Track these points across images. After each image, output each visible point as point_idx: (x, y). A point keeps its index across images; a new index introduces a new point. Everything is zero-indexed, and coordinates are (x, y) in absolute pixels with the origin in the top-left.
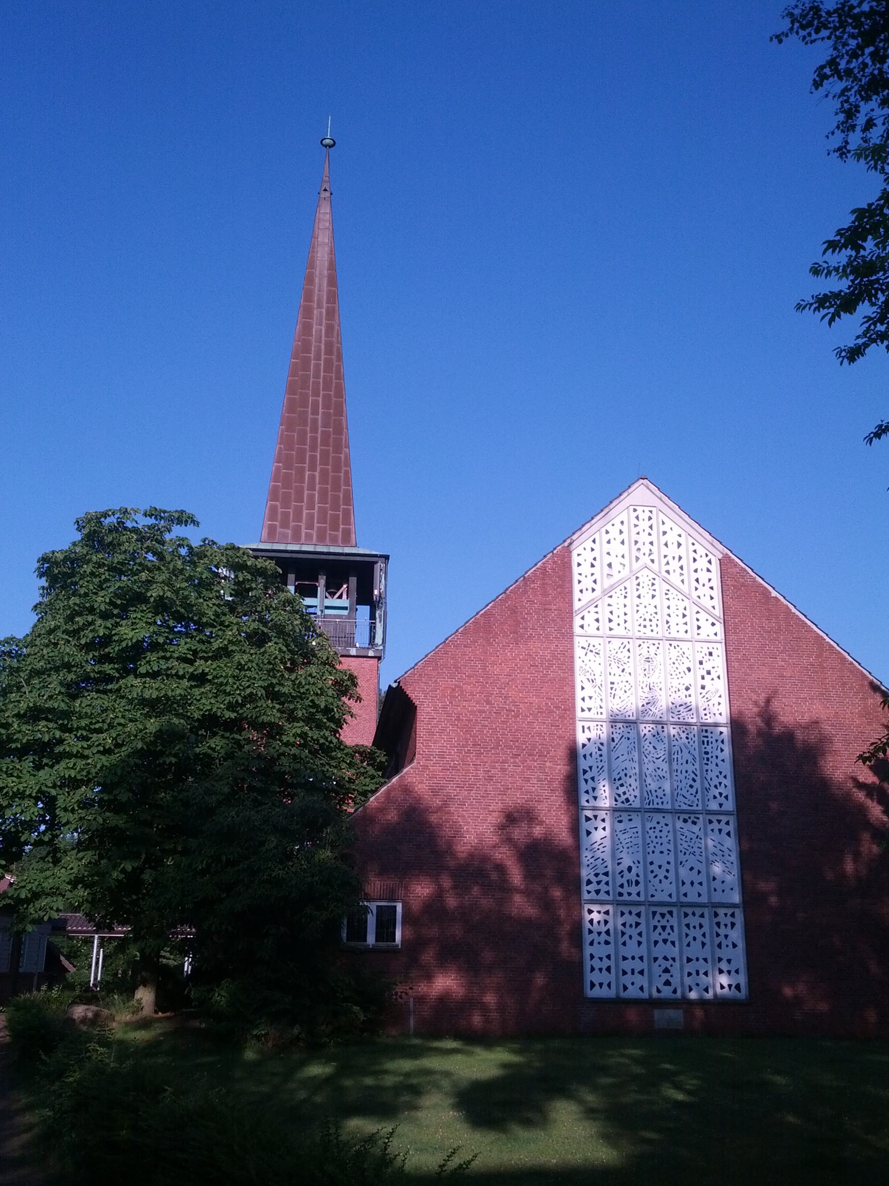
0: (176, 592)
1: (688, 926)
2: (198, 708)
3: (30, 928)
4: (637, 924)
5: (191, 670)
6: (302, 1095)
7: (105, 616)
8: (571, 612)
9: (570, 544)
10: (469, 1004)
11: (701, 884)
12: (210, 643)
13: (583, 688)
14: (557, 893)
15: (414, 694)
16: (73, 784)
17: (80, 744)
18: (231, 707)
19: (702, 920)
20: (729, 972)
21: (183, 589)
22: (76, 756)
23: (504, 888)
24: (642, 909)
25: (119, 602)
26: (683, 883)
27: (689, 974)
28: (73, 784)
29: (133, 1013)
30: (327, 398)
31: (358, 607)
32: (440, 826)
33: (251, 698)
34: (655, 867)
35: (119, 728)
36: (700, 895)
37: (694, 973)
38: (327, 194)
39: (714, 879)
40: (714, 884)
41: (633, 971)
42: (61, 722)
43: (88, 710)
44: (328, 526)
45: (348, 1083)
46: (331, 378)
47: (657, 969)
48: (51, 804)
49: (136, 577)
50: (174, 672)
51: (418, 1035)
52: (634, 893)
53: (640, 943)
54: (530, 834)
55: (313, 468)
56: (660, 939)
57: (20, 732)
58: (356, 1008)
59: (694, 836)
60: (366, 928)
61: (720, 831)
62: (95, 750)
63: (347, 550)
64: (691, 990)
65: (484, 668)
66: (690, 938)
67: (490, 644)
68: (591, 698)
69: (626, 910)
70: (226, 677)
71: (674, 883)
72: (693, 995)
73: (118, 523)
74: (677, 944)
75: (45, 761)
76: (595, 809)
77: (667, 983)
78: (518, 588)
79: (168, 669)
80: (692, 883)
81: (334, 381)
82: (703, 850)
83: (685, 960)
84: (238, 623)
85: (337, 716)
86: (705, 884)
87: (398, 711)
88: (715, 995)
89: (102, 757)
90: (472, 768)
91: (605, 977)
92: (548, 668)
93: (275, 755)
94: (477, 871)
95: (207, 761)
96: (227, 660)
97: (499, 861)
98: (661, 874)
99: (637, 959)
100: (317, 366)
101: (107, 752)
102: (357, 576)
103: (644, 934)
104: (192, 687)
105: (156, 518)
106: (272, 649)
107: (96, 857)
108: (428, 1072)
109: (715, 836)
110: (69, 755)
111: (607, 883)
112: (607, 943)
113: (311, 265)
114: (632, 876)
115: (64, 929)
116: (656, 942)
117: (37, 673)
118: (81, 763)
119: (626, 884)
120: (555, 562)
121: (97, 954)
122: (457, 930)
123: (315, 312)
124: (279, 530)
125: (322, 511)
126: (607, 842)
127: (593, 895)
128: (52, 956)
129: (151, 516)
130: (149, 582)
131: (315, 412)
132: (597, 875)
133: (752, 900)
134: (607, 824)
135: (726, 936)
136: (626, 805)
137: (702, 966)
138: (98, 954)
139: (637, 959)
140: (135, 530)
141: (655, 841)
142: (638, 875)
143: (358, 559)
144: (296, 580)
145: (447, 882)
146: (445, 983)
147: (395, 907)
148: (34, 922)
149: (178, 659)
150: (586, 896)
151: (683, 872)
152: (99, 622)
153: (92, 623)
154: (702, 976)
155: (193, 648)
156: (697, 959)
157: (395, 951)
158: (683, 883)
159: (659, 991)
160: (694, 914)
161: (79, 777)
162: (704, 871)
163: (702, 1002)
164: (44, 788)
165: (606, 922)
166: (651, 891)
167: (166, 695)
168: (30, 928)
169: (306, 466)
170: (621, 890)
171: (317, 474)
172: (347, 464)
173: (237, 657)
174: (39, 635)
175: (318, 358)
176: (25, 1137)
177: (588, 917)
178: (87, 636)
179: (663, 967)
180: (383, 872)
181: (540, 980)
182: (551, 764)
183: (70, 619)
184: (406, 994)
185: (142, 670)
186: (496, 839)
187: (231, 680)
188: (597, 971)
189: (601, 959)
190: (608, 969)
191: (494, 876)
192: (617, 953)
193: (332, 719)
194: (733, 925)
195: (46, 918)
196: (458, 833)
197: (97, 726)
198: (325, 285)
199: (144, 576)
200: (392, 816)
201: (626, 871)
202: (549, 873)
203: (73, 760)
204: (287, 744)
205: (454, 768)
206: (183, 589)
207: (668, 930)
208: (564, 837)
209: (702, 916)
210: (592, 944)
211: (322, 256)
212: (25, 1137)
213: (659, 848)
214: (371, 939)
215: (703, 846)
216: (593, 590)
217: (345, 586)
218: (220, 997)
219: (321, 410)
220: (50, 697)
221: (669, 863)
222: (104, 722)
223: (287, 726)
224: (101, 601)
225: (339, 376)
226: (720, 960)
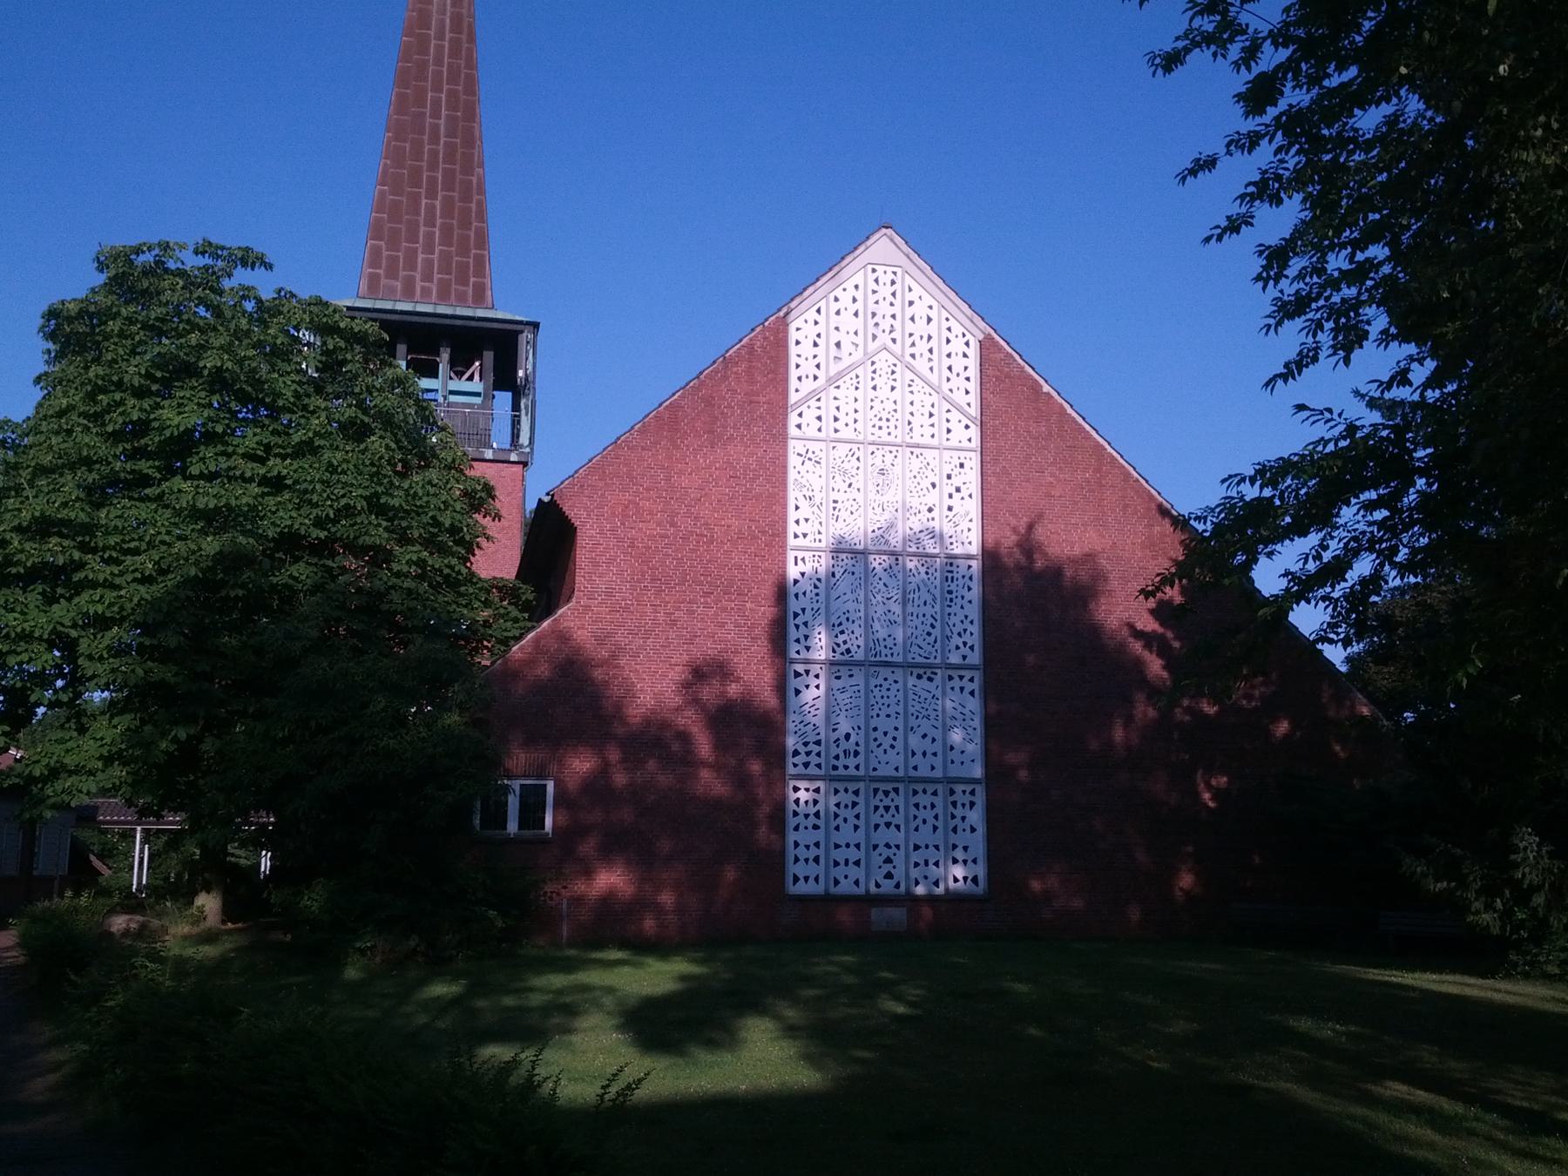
0: (240, 362)
3: (48, 814)
4: (855, 804)
6: (422, 1019)
7: (140, 393)
9: (787, 314)
10: (638, 905)
11: (935, 754)
14: (756, 767)
15: (575, 512)
16: (101, 623)
18: (319, 523)
20: (965, 862)
23: (686, 760)
24: (861, 785)
26: (914, 754)
27: (916, 865)
28: (101, 623)
30: (452, 94)
32: (606, 683)
33: (348, 511)
34: (879, 734)
35: (164, 548)
36: (933, 768)
39: (952, 748)
40: (951, 756)
41: (847, 862)
45: (481, 1003)
46: (459, 67)
47: (877, 859)
48: (69, 647)
51: (570, 945)
52: (852, 765)
53: (856, 827)
54: (723, 693)
55: (432, 194)
56: (881, 822)
57: (22, 551)
59: (930, 696)
61: (962, 689)
62: (129, 577)
63: (480, 313)
64: (917, 883)
65: (668, 479)
67: (677, 447)
72: (920, 890)
73: (156, 262)
76: (807, 662)
77: (889, 876)
78: (716, 371)
79: (230, 469)
80: (924, 754)
84: (326, 409)
88: (947, 889)
89: (142, 589)
90: (649, 609)
91: (812, 869)
92: (753, 480)
94: (655, 740)
95: (288, 595)
98: (887, 742)
100: (440, 48)
101: (146, 580)
103: (862, 816)
106: (377, 445)
107: (137, 723)
108: (585, 988)
109: (956, 695)
110: (94, 585)
111: (818, 754)
112: (816, 827)
114: (850, 745)
116: (877, 826)
118: (110, 595)
121: (140, 852)
124: (383, 281)
125: (446, 258)
126: (821, 704)
127: (801, 770)
128: (79, 855)
129: (203, 253)
130: (202, 348)
131: (436, 114)
132: (806, 744)
133: (996, 773)
134: (822, 682)
135: (963, 818)
136: (847, 657)
137: (932, 855)
138: (142, 851)
140: (181, 273)
143: (495, 325)
144: (408, 352)
145: (614, 755)
146: (611, 880)
148: (54, 807)
149: (244, 456)
150: (791, 770)
151: (914, 741)
152: (131, 402)
153: (122, 403)
157: (544, 841)
159: (878, 885)
160: (925, 791)
161: (108, 614)
163: (931, 899)
164: (60, 628)
167: (227, 505)
168: (48, 814)
169: (423, 191)
171: (438, 203)
175: (441, 36)
176: (52, 1078)
177: (793, 796)
178: (115, 422)
181: (730, 874)
183: (91, 397)
186: (678, 700)
189: (808, 847)
190: (816, 860)
191: (676, 747)
192: (946, 842)
193: (460, 542)
194: (972, 804)
196: (630, 692)
197: (132, 545)
199: (194, 338)
200: (543, 670)
204: (398, 575)
205: (626, 609)
212: (52, 1078)
213: (885, 711)
214: (512, 827)
222: (141, 539)
224: (133, 371)
225: (471, 64)
226: (955, 847)
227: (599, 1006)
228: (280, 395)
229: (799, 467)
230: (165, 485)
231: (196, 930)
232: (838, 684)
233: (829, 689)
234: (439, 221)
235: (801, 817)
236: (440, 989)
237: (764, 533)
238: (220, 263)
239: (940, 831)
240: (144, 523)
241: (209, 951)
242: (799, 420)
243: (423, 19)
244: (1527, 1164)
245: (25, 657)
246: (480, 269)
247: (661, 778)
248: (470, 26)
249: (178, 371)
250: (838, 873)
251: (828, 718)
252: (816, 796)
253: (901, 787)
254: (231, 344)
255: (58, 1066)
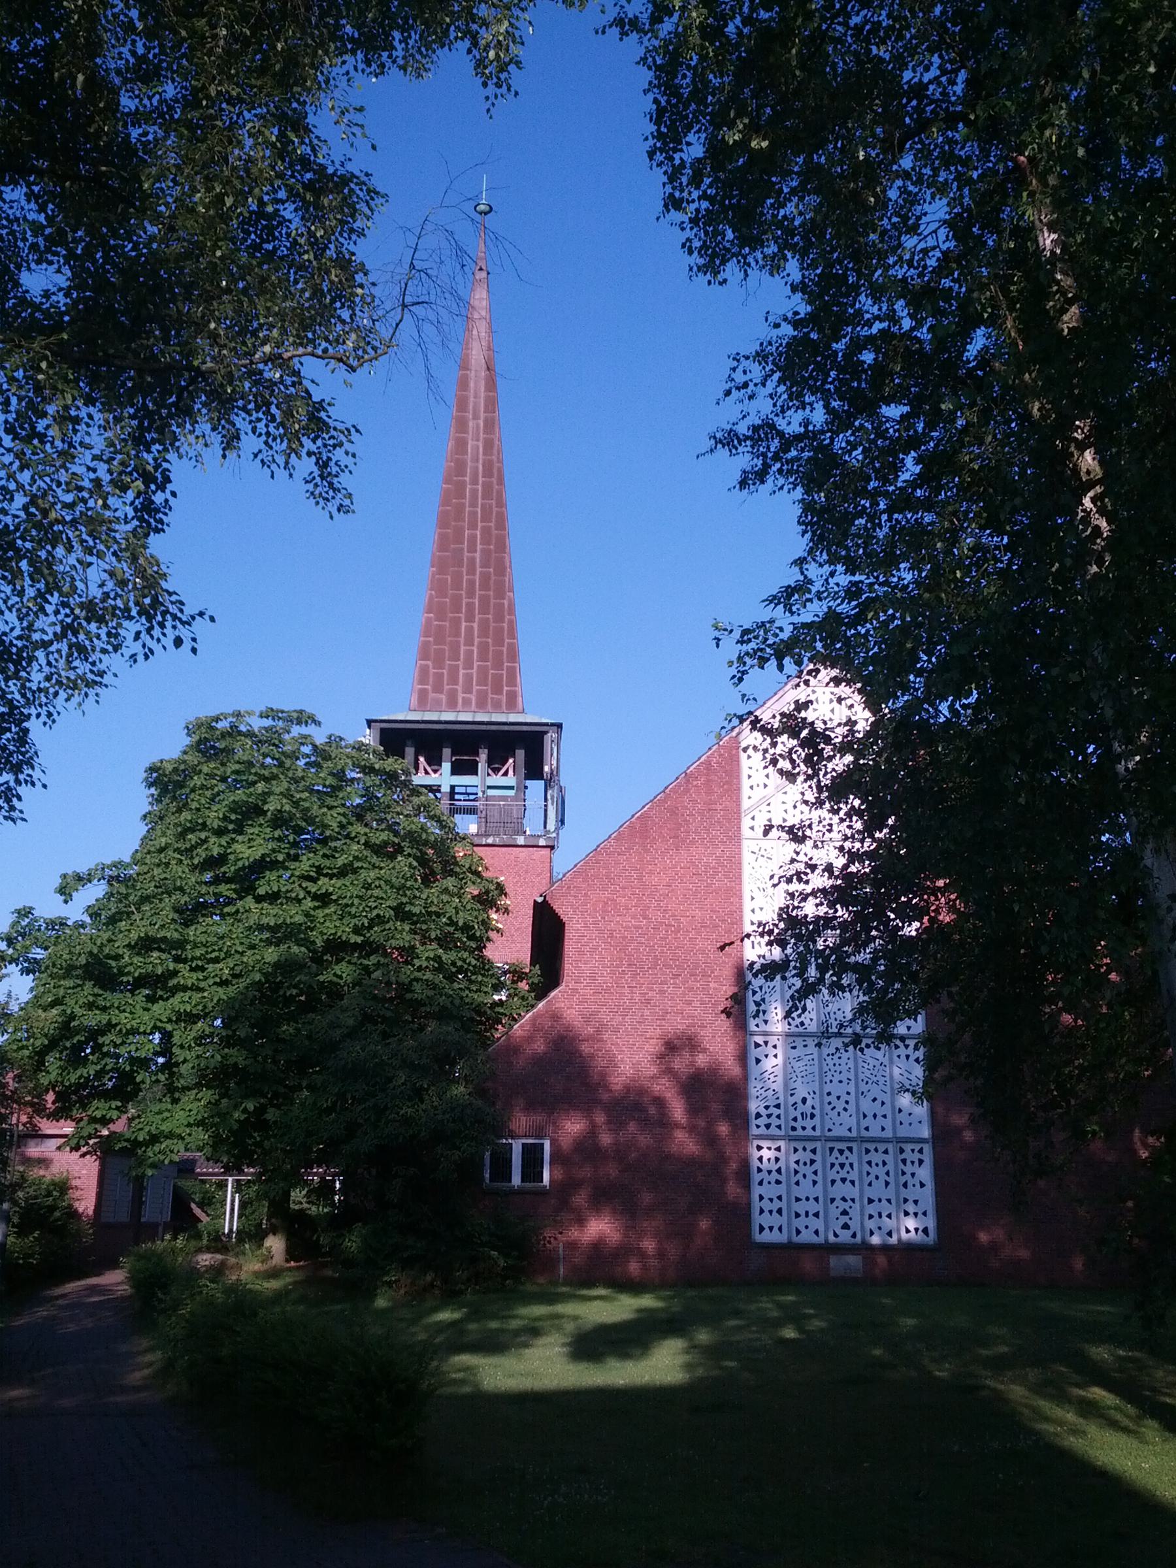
0: (296, 804)
1: (869, 1163)
2: (321, 933)
3: (149, 1172)
4: (813, 1162)
5: (313, 890)
6: (422, 1336)
7: (220, 832)
8: (738, 812)
9: (739, 734)
10: (624, 1252)
11: (885, 1116)
12: (334, 857)
13: (753, 898)
14: (723, 1129)
15: (562, 909)
16: (191, 1018)
17: (194, 975)
18: (357, 931)
19: (885, 1157)
20: (916, 1214)
21: (304, 800)
22: (191, 989)
23: (662, 1123)
24: (818, 1145)
25: (233, 817)
26: (865, 1116)
27: (871, 1217)
28: (191, 1018)
29: (262, 1262)
30: (486, 531)
31: (528, 783)
32: (592, 1056)
33: (380, 920)
34: (832, 1098)
35: (237, 956)
36: (883, 1129)
37: (876, 1215)
38: (484, 274)
39: (900, 1111)
40: (900, 1117)
41: (807, 1214)
42: (174, 952)
43: (203, 938)
44: (489, 688)
45: (472, 1326)
46: (491, 506)
47: (834, 1211)
48: (167, 1036)
49: (251, 790)
50: (294, 895)
51: (565, 1284)
52: (809, 1126)
53: (815, 1183)
54: (692, 1063)
55: (470, 618)
56: (838, 1178)
57: (131, 964)
58: (494, 1253)
59: (877, 1063)
60: (511, 1167)
61: (908, 1057)
62: (211, 981)
63: (513, 718)
64: (872, 1233)
65: (640, 878)
66: (872, 1177)
67: (647, 851)
68: (761, 909)
69: (799, 1146)
70: (351, 897)
71: (854, 1115)
72: (875, 1240)
73: (231, 727)
74: (857, 1183)
75: (160, 993)
76: (766, 1034)
77: (846, 1226)
78: (679, 785)
79: (288, 891)
80: (875, 1116)
81: (495, 509)
82: (887, 1079)
83: (866, 1201)
84: (366, 834)
85: (478, 934)
86: (889, 1116)
87: (548, 929)
88: (899, 1240)
89: (219, 989)
90: (627, 990)
91: (775, 1221)
92: (713, 876)
93: (407, 981)
94: (634, 1106)
95: (334, 992)
96: (353, 877)
97: (657, 1094)
98: (840, 1105)
99: (811, 1200)
100: (474, 492)
101: (224, 983)
102: (525, 748)
103: (820, 1173)
104: (315, 908)
105: (273, 719)
106: (402, 864)
107: (217, 1097)
108: (558, 1316)
109: (902, 1063)
110: (185, 989)
111: (778, 1117)
112: (778, 1182)
113: (465, 366)
114: (807, 1108)
115: (193, 1171)
116: (833, 1182)
117: (145, 899)
118: (197, 996)
119: (799, 1118)
120: (720, 755)
121: (232, 1199)
122: (612, 1171)
123: (471, 424)
124: (431, 695)
125: (483, 671)
126: (779, 1071)
127: (762, 1131)
128: (181, 1203)
129: (267, 717)
130: (266, 795)
131: (472, 549)
132: (767, 1107)
133: (942, 1135)
134: (779, 1051)
135: (913, 1175)
136: (801, 1029)
137: (886, 1209)
138: (233, 1201)
139: (811, 1200)
140: (250, 734)
141: (833, 1069)
142: (813, 1107)
143: (525, 728)
144: (453, 754)
145: (600, 1118)
146: (600, 1228)
147: (543, 1144)
148: (153, 1166)
149: (299, 877)
150: (754, 1131)
151: (866, 1105)
152: (213, 839)
153: (205, 841)
154: (884, 1218)
155: (317, 864)
156: (880, 1200)
157: (543, 1192)
158: (865, 1116)
159: (836, 1235)
160: (876, 1150)
161: (195, 1012)
162: (888, 1105)
163: (885, 1248)
164: (159, 1024)
165: (777, 1160)
166: (829, 1125)
167: (284, 922)
168: (149, 1172)
169: (462, 616)
170: (793, 1124)
171: (475, 625)
172: (512, 611)
173: (363, 873)
174: (149, 852)
175: (475, 481)
176: (146, 1372)
177: (756, 1154)
178: (201, 854)
179: (841, 1210)
180: (530, 1107)
181: (704, 1224)
182: (715, 985)
183: (182, 836)
184: (555, 1239)
185: (261, 891)
186: (654, 1070)
187: (356, 901)
188: (766, 1213)
189: (771, 1200)
190: (780, 1211)
191: (652, 1111)
192: (825, 1196)
193: (472, 938)
194: (921, 1162)
195: (166, 1162)
196: (612, 1060)
197: (213, 955)
198: (483, 389)
199: (261, 787)
200: (540, 1046)
201: (800, 1104)
202: (715, 1107)
203: (188, 994)
204: (420, 969)
205: (607, 990)
206: (304, 800)
207: (847, 1168)
208: (732, 1068)
209: (886, 1152)
210: (761, 1183)
211: (477, 356)
212: (146, 1372)
213: (837, 1077)
214: (516, 1180)
215: (887, 1074)
216: (765, 786)
217: (511, 761)
218: (352, 1243)
219: (479, 547)
220: (163, 926)
221: (848, 1093)
222: (220, 950)
223: (420, 949)
224: (213, 818)
225: (501, 504)
226: (906, 1201)
227: (559, 1328)
228: (326, 826)
229: (753, 863)
230: (240, 904)
231: (266, 1267)
232: (795, 1053)
233: (787, 1061)
234: (476, 641)
235: (765, 1173)
236: (445, 1316)
237: (723, 921)
238: (280, 723)
239: (892, 1186)
240: (222, 938)
241: (274, 1284)
242: (752, 823)
243: (460, 468)
244: (1119, 1434)
245: (133, 1047)
246: (512, 680)
247: (641, 1138)
248: (500, 471)
249: (250, 812)
250: (800, 1223)
251: (786, 1085)
252: (777, 1154)
253: (854, 1145)
254: (289, 789)
255: (150, 1364)
